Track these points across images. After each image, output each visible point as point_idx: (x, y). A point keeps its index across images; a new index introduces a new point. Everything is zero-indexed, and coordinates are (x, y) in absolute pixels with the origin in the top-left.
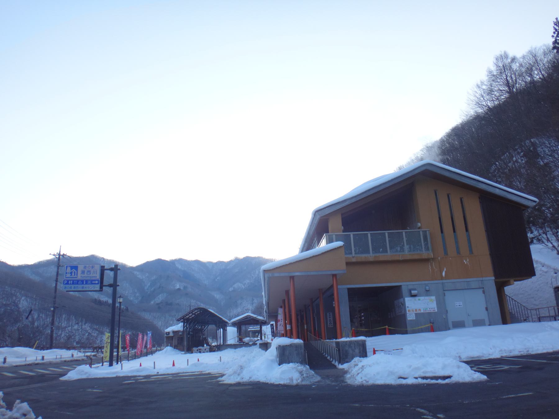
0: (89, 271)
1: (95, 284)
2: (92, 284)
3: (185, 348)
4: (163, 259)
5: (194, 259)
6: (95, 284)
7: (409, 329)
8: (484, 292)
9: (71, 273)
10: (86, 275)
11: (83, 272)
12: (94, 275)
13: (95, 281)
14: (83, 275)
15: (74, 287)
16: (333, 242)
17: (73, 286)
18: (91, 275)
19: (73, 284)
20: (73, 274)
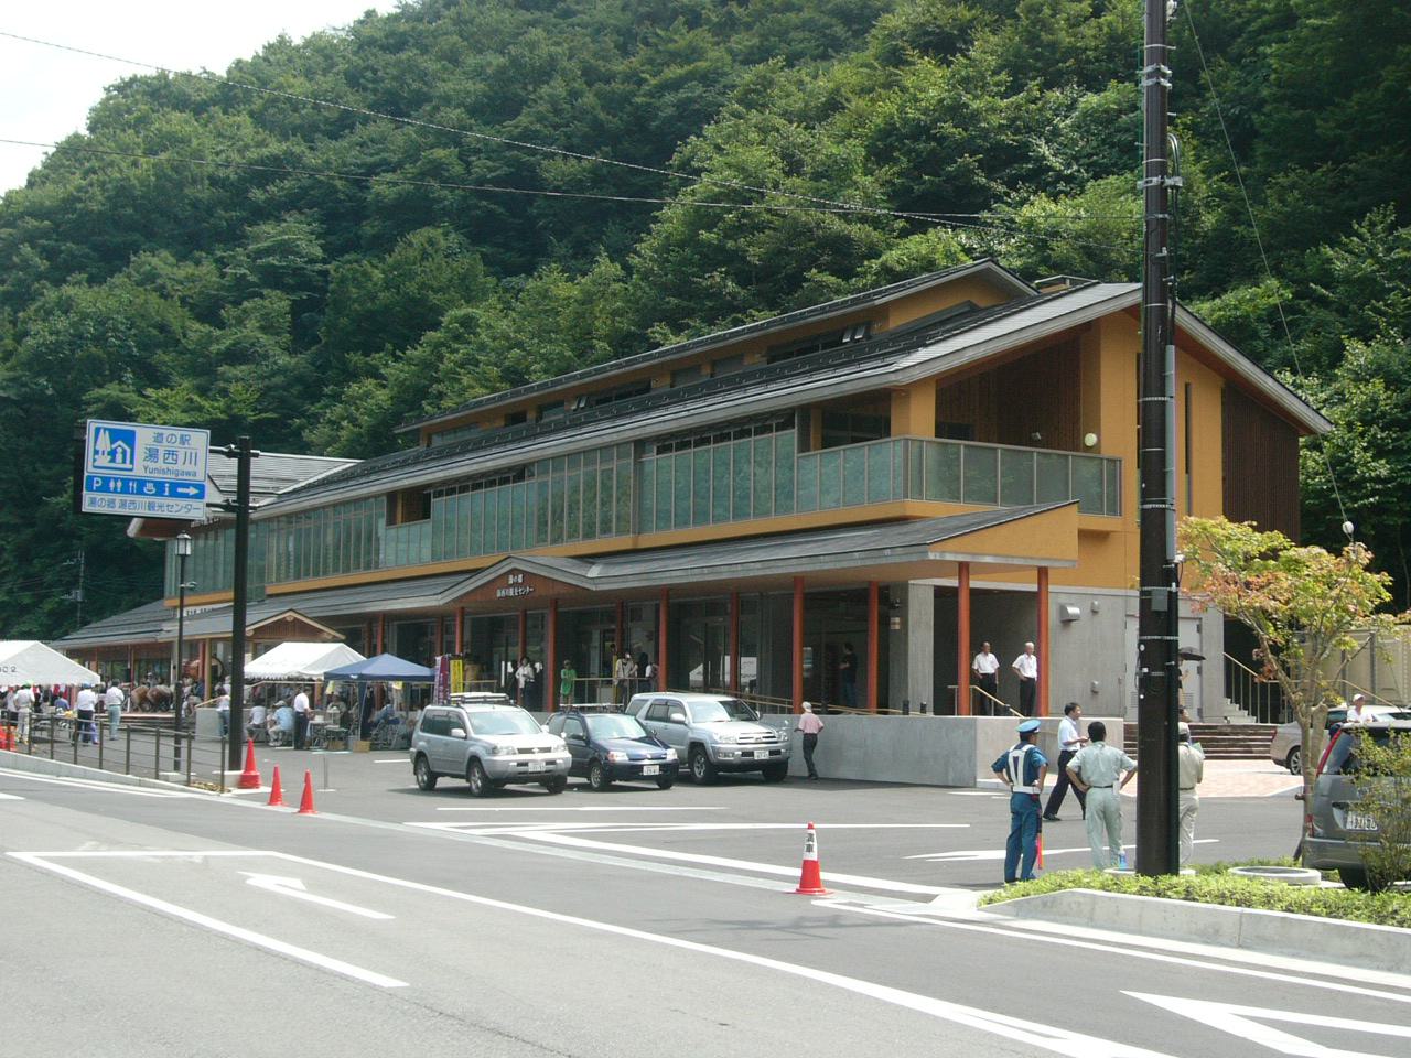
0: (171, 453)
1: (186, 496)
2: (174, 494)
3: (269, 71)
4: (1250, 1038)
5: (249, 48)
6: (186, 496)
7: (385, 498)
8: (1199, 629)
9: (113, 453)
10: (160, 464)
11: (152, 454)
12: (188, 467)
13: (187, 486)
14: (152, 465)
15: (123, 504)
16: (809, 450)
17: (118, 498)
18: (179, 467)
19: (125, 490)
20: (119, 457)
